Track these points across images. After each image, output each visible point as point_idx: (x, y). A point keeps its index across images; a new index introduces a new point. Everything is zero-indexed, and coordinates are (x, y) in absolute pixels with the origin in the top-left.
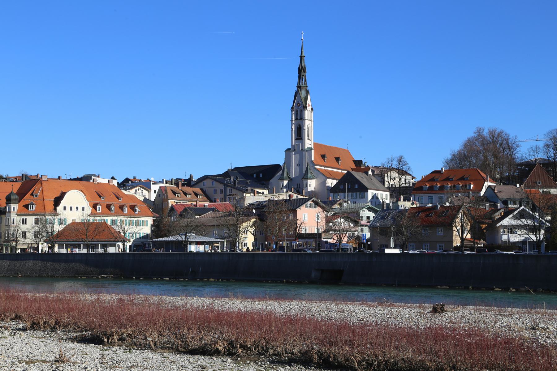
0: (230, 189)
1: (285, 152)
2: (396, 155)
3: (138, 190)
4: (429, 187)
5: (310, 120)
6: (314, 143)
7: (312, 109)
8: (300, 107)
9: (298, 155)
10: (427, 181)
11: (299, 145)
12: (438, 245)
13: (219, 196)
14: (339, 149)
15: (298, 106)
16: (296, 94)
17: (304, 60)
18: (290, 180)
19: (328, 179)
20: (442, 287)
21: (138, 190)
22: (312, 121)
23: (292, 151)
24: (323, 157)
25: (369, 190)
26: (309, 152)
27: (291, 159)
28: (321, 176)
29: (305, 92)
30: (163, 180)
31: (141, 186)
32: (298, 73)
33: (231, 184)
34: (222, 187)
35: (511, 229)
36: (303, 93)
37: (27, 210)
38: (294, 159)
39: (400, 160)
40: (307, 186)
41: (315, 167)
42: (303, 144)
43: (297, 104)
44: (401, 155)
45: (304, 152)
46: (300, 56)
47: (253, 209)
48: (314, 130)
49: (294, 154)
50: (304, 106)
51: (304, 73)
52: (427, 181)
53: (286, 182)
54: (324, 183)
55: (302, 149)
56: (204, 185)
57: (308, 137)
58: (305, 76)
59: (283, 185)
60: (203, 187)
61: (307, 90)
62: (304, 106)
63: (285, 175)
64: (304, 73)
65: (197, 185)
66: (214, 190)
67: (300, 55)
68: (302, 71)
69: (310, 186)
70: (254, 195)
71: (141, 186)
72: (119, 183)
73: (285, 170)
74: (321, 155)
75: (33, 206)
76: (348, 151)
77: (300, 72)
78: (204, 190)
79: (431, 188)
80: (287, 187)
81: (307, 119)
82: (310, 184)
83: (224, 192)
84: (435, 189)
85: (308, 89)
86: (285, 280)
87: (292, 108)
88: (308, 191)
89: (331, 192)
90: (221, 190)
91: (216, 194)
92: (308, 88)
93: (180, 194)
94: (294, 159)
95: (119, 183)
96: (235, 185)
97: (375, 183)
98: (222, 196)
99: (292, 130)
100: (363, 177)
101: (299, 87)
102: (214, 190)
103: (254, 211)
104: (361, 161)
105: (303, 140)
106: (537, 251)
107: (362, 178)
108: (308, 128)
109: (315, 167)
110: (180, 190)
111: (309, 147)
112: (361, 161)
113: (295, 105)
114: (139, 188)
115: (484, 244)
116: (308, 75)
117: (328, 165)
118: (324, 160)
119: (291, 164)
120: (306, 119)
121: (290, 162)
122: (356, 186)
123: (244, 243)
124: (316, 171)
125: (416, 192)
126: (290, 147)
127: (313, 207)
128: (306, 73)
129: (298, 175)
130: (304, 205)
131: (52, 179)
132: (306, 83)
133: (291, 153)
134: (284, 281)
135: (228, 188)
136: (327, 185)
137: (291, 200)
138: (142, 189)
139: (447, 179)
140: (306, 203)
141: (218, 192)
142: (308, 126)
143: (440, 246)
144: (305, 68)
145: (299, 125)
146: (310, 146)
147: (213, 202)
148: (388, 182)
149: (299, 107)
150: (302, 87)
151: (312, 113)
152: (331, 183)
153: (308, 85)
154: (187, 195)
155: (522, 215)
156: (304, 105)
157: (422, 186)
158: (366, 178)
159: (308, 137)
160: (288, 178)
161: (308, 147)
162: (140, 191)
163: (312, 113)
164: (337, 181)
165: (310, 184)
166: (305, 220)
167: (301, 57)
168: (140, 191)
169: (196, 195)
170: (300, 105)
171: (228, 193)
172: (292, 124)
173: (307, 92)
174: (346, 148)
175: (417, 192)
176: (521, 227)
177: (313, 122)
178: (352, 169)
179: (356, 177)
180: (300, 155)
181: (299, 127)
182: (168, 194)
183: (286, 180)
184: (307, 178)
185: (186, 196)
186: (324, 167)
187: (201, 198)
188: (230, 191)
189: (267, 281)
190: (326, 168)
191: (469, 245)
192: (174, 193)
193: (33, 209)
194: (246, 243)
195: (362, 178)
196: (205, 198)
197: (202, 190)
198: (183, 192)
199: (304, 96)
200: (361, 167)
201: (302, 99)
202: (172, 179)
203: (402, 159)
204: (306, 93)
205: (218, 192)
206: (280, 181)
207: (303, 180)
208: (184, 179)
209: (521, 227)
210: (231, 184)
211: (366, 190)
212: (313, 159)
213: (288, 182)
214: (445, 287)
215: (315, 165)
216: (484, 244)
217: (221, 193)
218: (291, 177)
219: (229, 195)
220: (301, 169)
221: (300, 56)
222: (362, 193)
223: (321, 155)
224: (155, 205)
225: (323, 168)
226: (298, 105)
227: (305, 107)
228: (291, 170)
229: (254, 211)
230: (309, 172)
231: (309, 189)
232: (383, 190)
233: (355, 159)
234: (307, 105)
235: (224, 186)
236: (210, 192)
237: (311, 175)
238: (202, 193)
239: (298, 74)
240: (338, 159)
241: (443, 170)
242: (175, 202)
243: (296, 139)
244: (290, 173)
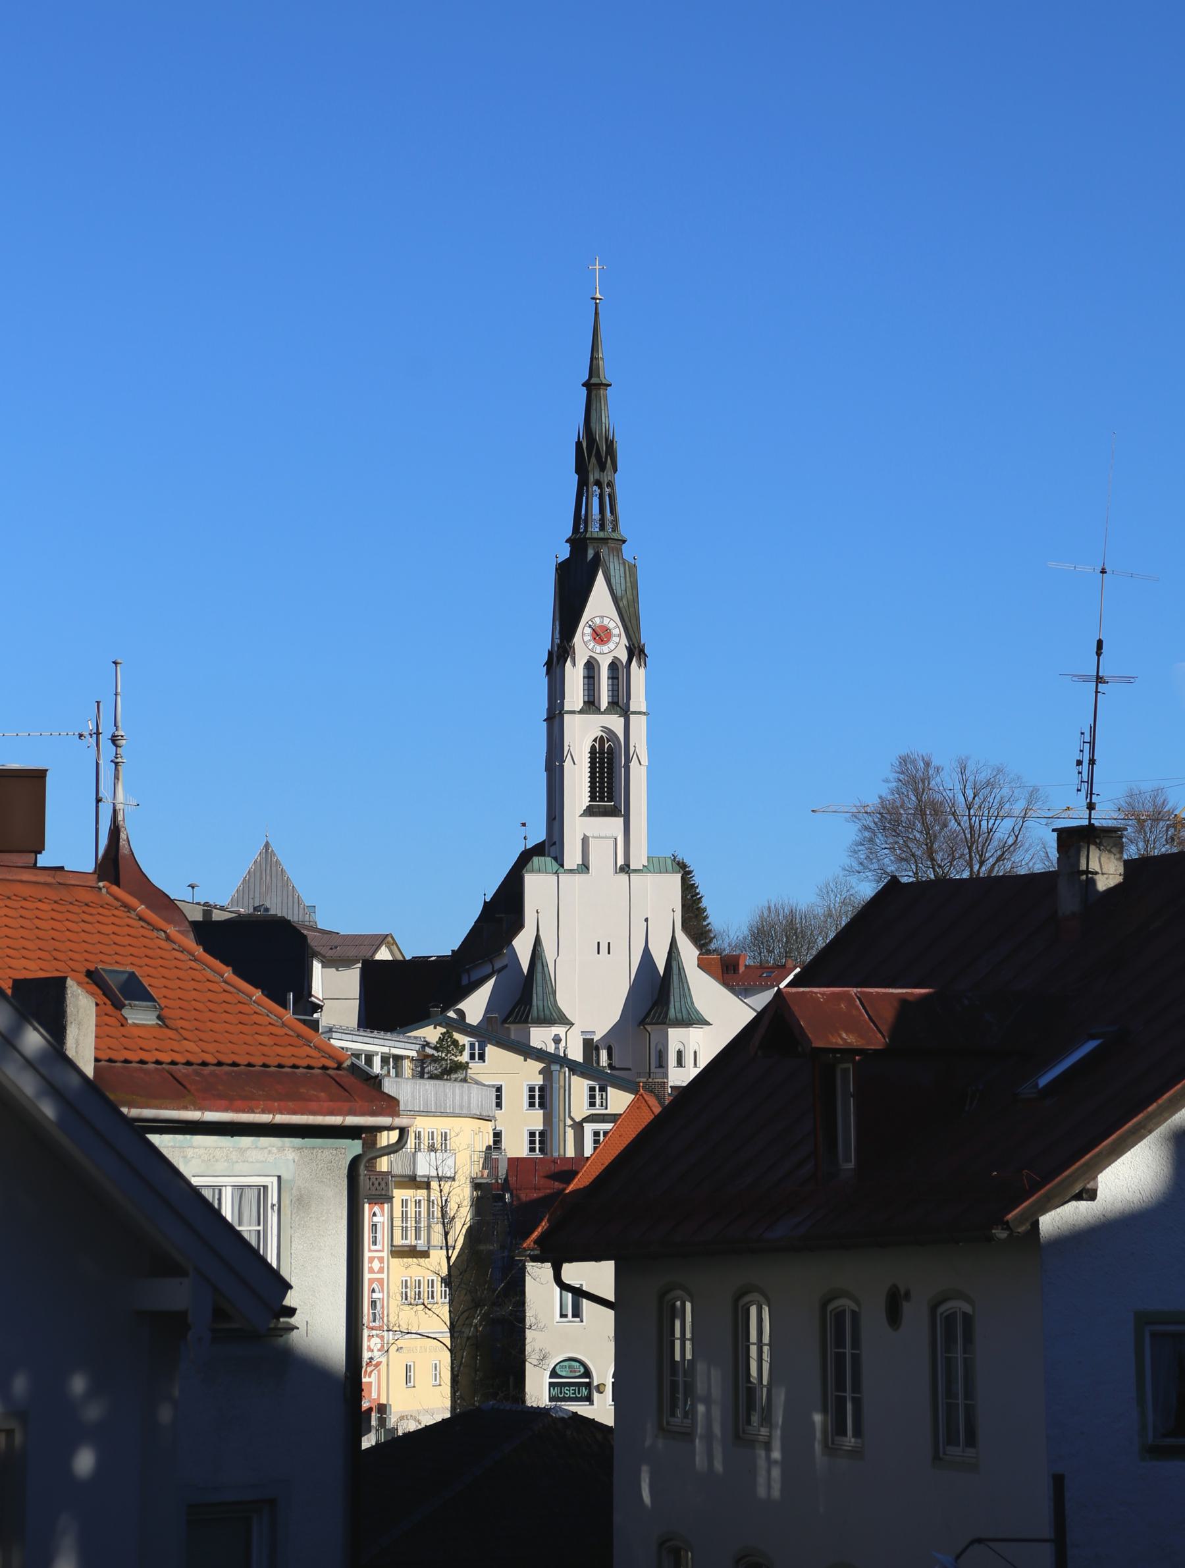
8: (611, 645)
32: (577, 472)
37: (282, 854)
46: (584, 385)
58: (610, 484)
68: (593, 460)
72: (433, 1026)
77: (581, 468)
82: (695, 1052)
95: (433, 1026)
106: (448, 1068)
128: (615, 470)
131: (182, 911)
144: (610, 445)
165: (695, 1052)
167: (594, 387)
181: (602, 752)
193: (406, 1239)
221: (584, 385)
224: (91, 904)
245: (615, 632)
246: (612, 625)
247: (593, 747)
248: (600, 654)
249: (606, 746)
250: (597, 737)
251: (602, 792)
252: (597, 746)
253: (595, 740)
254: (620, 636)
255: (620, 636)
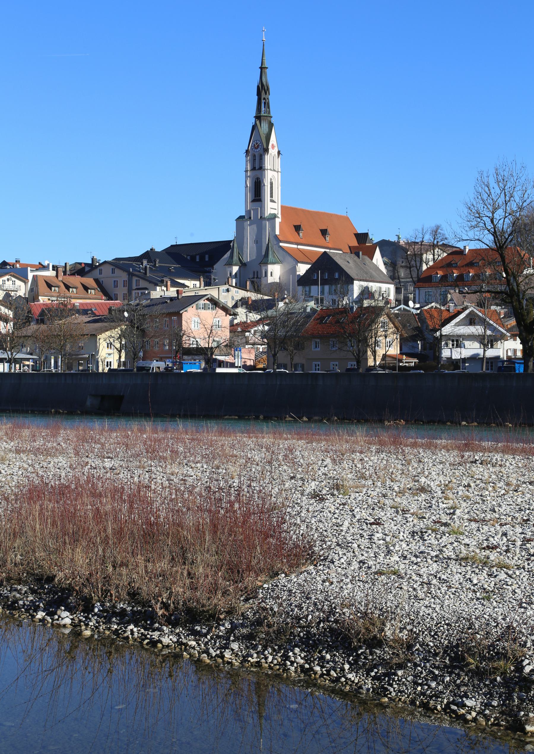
0: (137, 280)
1: (235, 223)
2: (430, 224)
3: (8, 280)
4: (457, 276)
5: (274, 170)
6: (282, 207)
7: (279, 153)
8: (259, 149)
9: (254, 227)
10: (441, 267)
11: (256, 211)
12: (314, 363)
13: (122, 290)
14: (331, 215)
15: (256, 148)
16: (254, 127)
17: (265, 74)
18: (243, 265)
19: (299, 264)
20: (231, 417)
21: (8, 280)
22: (278, 172)
23: (247, 220)
24: (298, 228)
25: (355, 282)
26: (271, 221)
27: (245, 233)
28: (290, 259)
29: (267, 125)
30: (48, 264)
31: (12, 273)
33: (140, 272)
34: (124, 276)
35: (457, 341)
36: (264, 127)
38: (250, 231)
39: (435, 232)
40: (266, 275)
41: (281, 244)
42: (262, 208)
43: (255, 145)
44: (438, 224)
45: (264, 222)
47: (124, 311)
48: (281, 186)
49: (250, 225)
50: (264, 149)
51: (266, 94)
52: (441, 267)
53: (235, 269)
54: (294, 270)
55: (261, 217)
56: (100, 274)
57: (271, 196)
58: (268, 99)
59: (231, 274)
60: (98, 276)
61: (270, 122)
62: (264, 149)
63: (235, 258)
64: (266, 94)
65: (91, 273)
66: (115, 281)
67: (260, 66)
68: (263, 91)
69: (271, 275)
70: (167, 290)
71: (12, 273)
73: (235, 249)
74: (295, 226)
76: (347, 219)
77: (259, 94)
78: (101, 280)
79: (444, 278)
80: (238, 276)
81: (269, 168)
82: (271, 273)
83: (128, 284)
84: (434, 280)
85: (273, 120)
86: (53, 410)
87: (247, 151)
88: (269, 282)
89: (299, 285)
90: (124, 281)
91: (117, 287)
92: (272, 119)
93: (58, 287)
94: (250, 231)
96: (146, 273)
97: (371, 270)
98: (125, 290)
99: (247, 186)
100: (350, 261)
101: (258, 117)
102: (115, 281)
103: (126, 314)
104: (366, 235)
105: (263, 202)
107: (348, 262)
108: (271, 184)
109: (281, 244)
110: (60, 281)
111: (272, 213)
112: (366, 235)
113: (252, 146)
114: (9, 277)
115: (415, 362)
116: (273, 98)
117: (304, 242)
118: (299, 234)
119: (245, 240)
120: (267, 169)
121: (244, 237)
122: (337, 276)
123: (107, 362)
124: (281, 251)
125: (421, 284)
126: (243, 214)
127: (209, 309)
128: (269, 94)
129: (254, 258)
130: (194, 305)
132: (269, 111)
133: (245, 223)
134: (51, 412)
135: (135, 279)
136: (298, 273)
137: (180, 297)
138: (14, 279)
139: (471, 264)
140: (197, 303)
141: (120, 284)
142: (271, 179)
143: (316, 365)
145: (258, 179)
146: (273, 212)
147: (112, 300)
148: (416, 267)
149: (257, 150)
150: (262, 118)
151: (279, 159)
152: (302, 269)
153: (272, 114)
154: (89, 291)
155: (471, 320)
156: (265, 146)
157: (431, 276)
158: (355, 261)
159: (271, 196)
160: (239, 262)
161: (270, 214)
162: (11, 282)
163: (279, 159)
164: (309, 266)
165: (271, 273)
166: (196, 328)
167: (262, 68)
168: (11, 282)
169: (86, 288)
170: (258, 146)
171: (134, 287)
172: (246, 177)
173: (271, 125)
174: (344, 214)
175: (424, 284)
176: (471, 337)
177: (280, 173)
178: (350, 247)
179: (337, 261)
180: (257, 227)
182: (39, 287)
183: (236, 265)
184: (266, 263)
185: (69, 291)
186: (298, 244)
187: (93, 293)
188: (137, 283)
189: (27, 412)
190: (300, 247)
191: (392, 363)
192: (50, 286)
194: (110, 362)
195: (348, 262)
196: (101, 293)
197: (97, 281)
198: (64, 284)
199: (265, 132)
200: (365, 243)
201: (262, 137)
202: (66, 264)
203: (439, 231)
204: (269, 127)
205: (120, 284)
206: (227, 266)
207: (262, 265)
208: (84, 263)
209: (471, 337)
210: (140, 272)
211: (350, 280)
212: (277, 233)
213: (240, 268)
214: (233, 417)
215: (281, 242)
216: (415, 362)
217: (124, 286)
218: (245, 261)
219: (135, 290)
220: (259, 249)
222: (307, 288)
223: (295, 226)
225: (295, 246)
226: (256, 147)
227: (266, 150)
228: (245, 249)
229: (126, 314)
230: (270, 252)
231: (270, 280)
232: (381, 280)
233: (359, 232)
234: (270, 147)
235: (129, 276)
236: (108, 283)
237: (274, 257)
238: (96, 286)
239: (257, 97)
240: (324, 232)
241: (467, 250)
242: (49, 300)
243: (253, 201)
244: (243, 254)
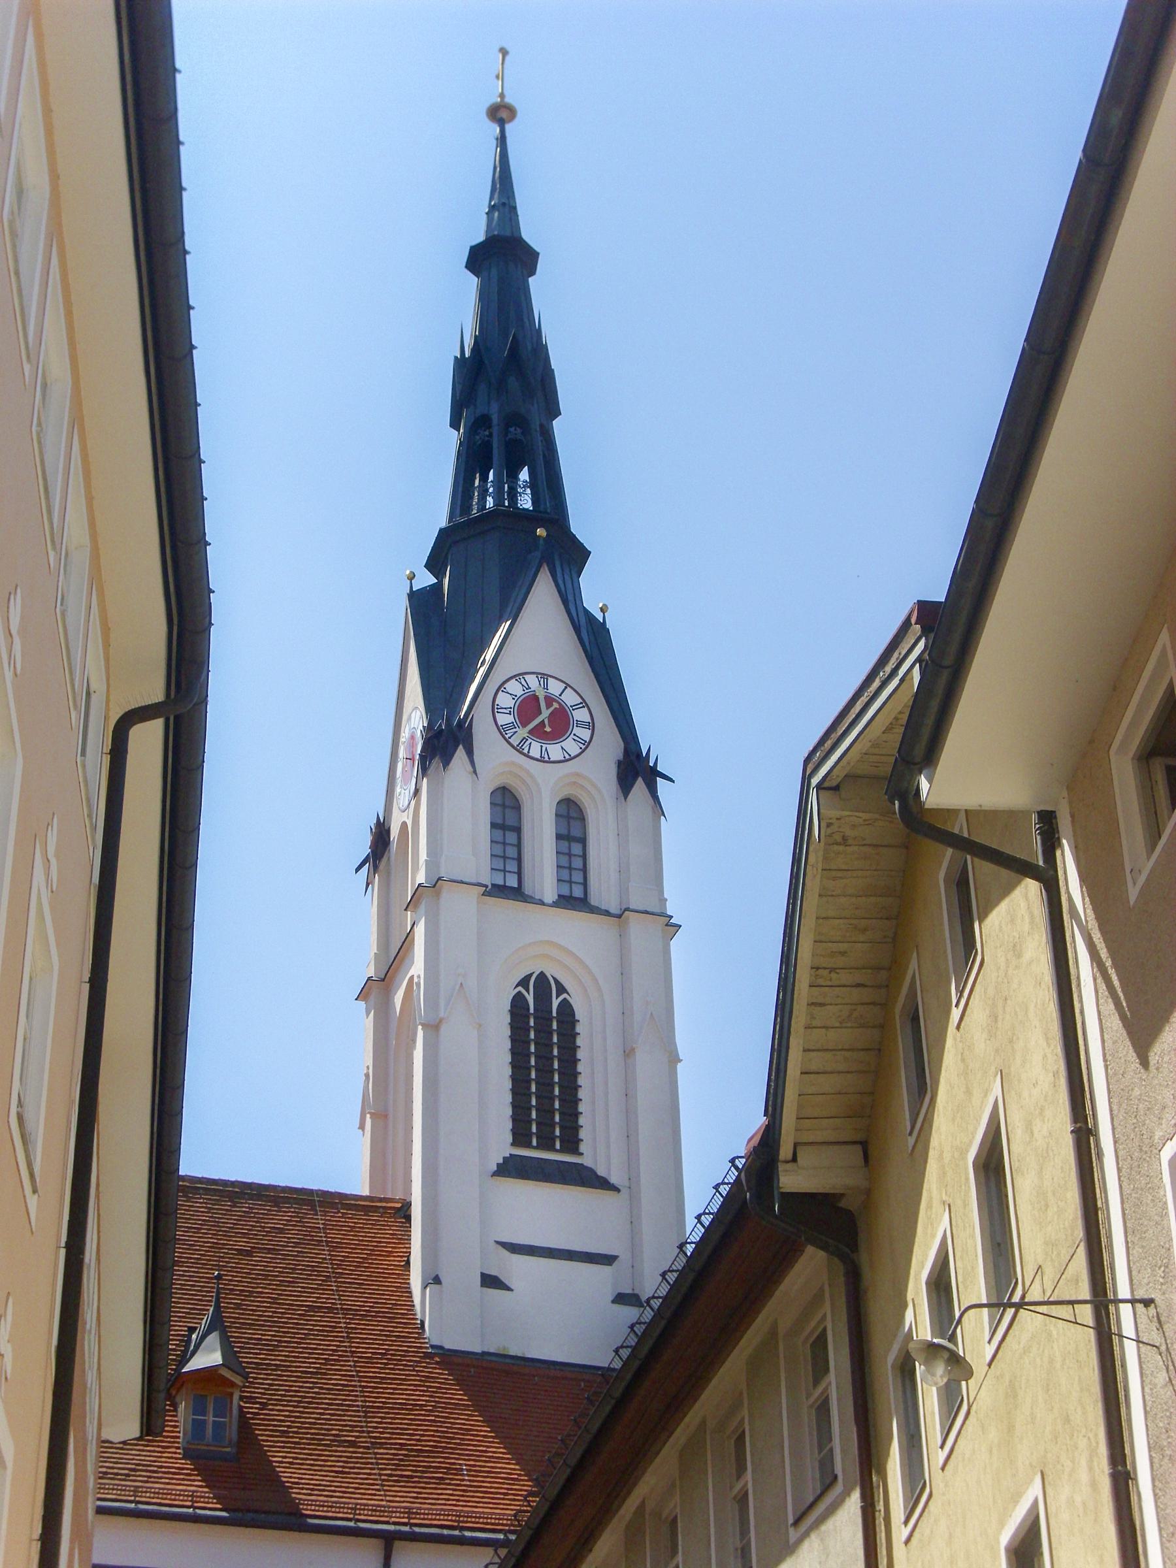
75: (179, 1437)
245: (581, 715)
246: (570, 698)
247: (518, 1004)
248: (541, 760)
249: (555, 1003)
250: (531, 975)
251: (546, 1123)
252: (530, 999)
253: (524, 983)
254: (591, 726)
255: (591, 726)
